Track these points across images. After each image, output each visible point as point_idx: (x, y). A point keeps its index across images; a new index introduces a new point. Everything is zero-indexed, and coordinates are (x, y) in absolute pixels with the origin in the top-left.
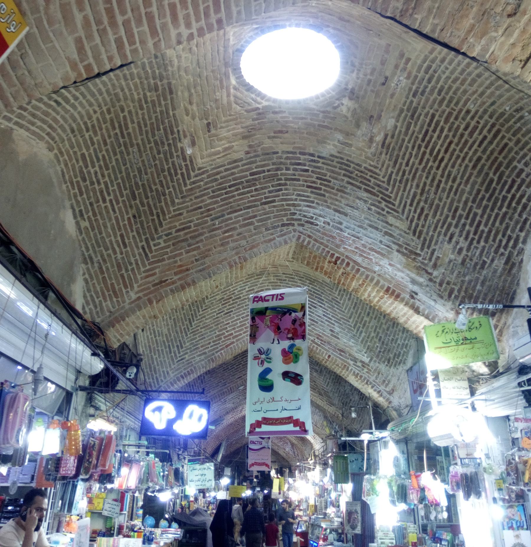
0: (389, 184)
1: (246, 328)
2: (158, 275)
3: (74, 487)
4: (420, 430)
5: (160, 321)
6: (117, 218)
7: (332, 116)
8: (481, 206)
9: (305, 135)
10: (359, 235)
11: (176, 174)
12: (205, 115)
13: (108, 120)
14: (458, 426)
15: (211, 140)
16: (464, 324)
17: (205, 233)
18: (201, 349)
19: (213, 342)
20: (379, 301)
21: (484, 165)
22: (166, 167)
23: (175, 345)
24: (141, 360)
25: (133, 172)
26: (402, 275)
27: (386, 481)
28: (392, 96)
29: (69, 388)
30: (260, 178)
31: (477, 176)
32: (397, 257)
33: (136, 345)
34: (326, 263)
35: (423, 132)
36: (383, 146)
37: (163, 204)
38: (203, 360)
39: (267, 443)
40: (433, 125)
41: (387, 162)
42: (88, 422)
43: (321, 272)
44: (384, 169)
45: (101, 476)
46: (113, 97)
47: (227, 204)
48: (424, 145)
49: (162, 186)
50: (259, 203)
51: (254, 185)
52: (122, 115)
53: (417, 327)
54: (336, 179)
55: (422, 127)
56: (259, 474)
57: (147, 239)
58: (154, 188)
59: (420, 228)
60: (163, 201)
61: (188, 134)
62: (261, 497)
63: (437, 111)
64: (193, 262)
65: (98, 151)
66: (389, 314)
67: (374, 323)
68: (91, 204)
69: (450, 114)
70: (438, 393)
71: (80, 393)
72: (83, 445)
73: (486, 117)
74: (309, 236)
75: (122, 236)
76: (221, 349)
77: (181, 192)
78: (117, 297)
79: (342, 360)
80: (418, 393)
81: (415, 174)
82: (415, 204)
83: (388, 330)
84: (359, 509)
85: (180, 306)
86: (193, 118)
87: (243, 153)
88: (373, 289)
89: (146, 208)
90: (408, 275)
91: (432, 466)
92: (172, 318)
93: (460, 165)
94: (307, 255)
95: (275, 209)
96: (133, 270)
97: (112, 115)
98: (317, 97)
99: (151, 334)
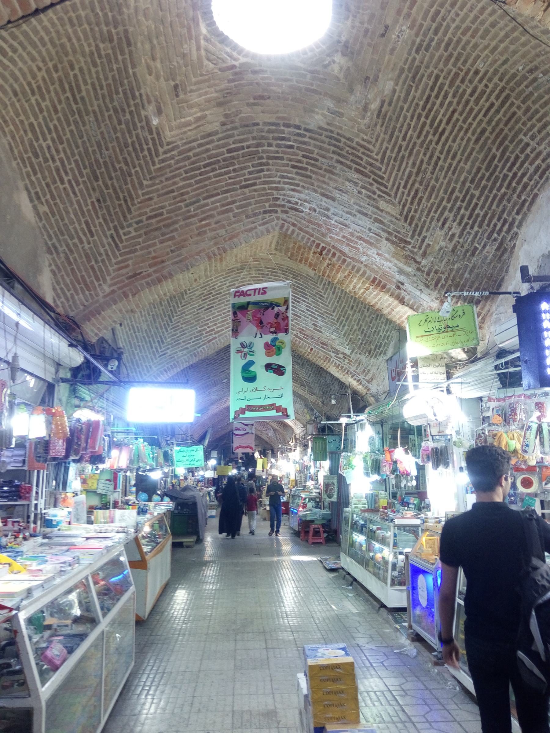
0: (382, 163)
1: (227, 324)
2: (131, 267)
3: (67, 469)
4: (396, 412)
5: (138, 317)
6: (78, 202)
7: (321, 76)
8: (480, 186)
9: (290, 102)
10: (347, 222)
11: (142, 150)
12: (172, 75)
13: (56, 79)
14: (432, 407)
15: (180, 107)
16: (448, 312)
17: (179, 220)
18: (183, 344)
19: (195, 337)
20: (364, 292)
21: (488, 138)
22: (129, 141)
23: (156, 340)
24: (122, 353)
25: (92, 147)
26: (390, 265)
27: (362, 456)
28: (393, 50)
29: (50, 380)
30: (238, 157)
31: (479, 152)
32: (386, 246)
33: (115, 340)
34: (311, 254)
35: (425, 98)
36: (378, 116)
37: (130, 186)
38: (186, 355)
39: (251, 429)
40: (436, 89)
41: (382, 135)
42: (75, 411)
43: (306, 264)
44: (378, 145)
45: (91, 457)
46: (59, 48)
47: (202, 187)
48: (424, 114)
49: (127, 164)
50: (238, 186)
51: (233, 164)
52: (71, 73)
53: (401, 317)
54: (324, 157)
55: (424, 92)
56: (244, 456)
57: (115, 227)
58: (117, 166)
59: (412, 213)
60: (129, 182)
61: (152, 99)
62: (246, 475)
63: (442, 71)
64: (168, 254)
65: (48, 120)
66: (373, 306)
67: (357, 316)
68: (48, 185)
69: (457, 75)
70: (416, 378)
71: (62, 384)
72: (70, 429)
73: (496, 79)
74: (294, 225)
75: (87, 223)
76: (204, 344)
77: (150, 172)
78: (89, 290)
79: (324, 352)
80: (396, 379)
81: (412, 150)
82: (409, 186)
83: (371, 323)
84: (335, 481)
85: (158, 300)
86: (158, 78)
87: (218, 124)
88: (359, 280)
89: (111, 191)
90: (395, 265)
91: (405, 442)
92: (151, 314)
93: (462, 139)
94: (291, 245)
95: (256, 193)
96: (103, 261)
97: (61, 73)
98: (305, 53)
99: (130, 330)
